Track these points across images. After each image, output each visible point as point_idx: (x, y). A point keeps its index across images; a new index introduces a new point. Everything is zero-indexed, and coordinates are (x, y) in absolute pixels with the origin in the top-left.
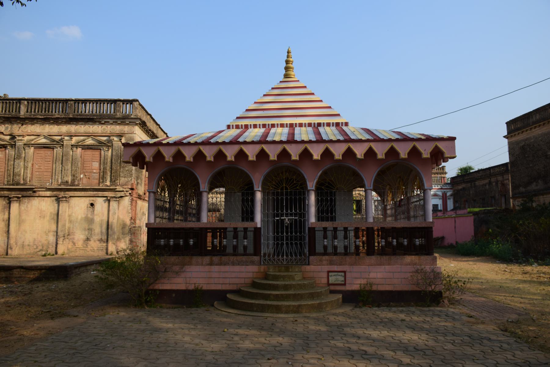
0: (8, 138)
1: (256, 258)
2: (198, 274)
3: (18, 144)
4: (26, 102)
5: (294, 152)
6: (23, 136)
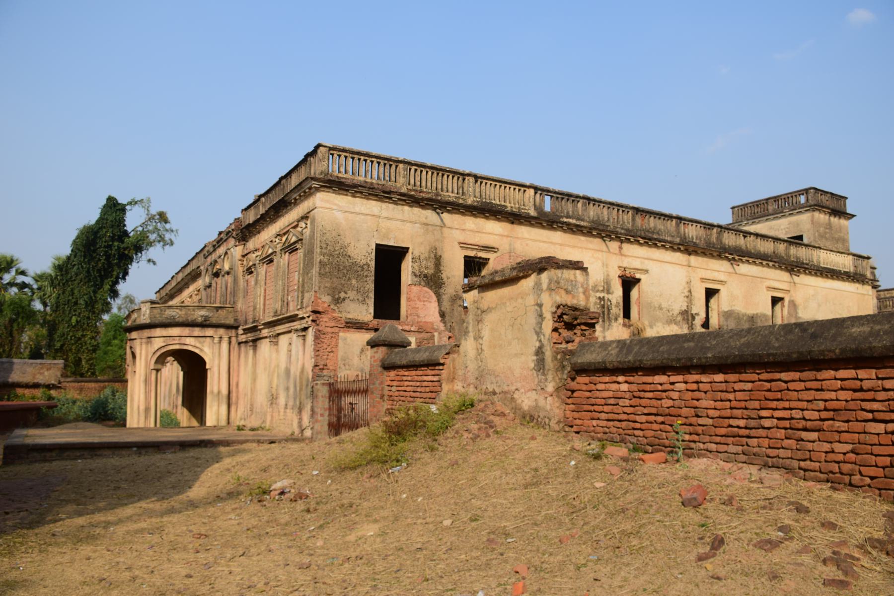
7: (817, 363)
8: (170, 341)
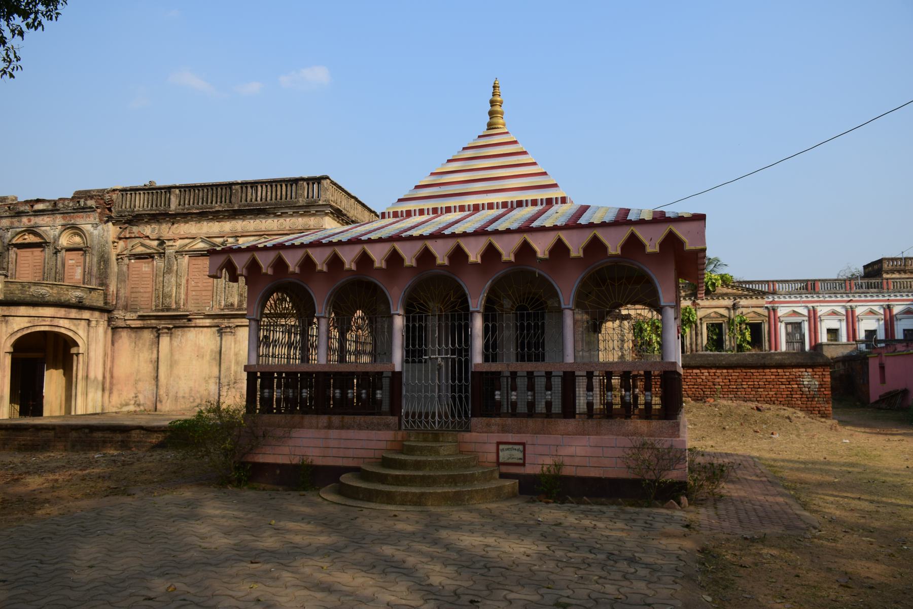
0: (156, 243)
1: (393, 420)
2: (312, 442)
3: (170, 251)
4: (177, 191)
5: (541, 246)
6: (174, 240)
7: (764, 367)
8: (37, 321)
